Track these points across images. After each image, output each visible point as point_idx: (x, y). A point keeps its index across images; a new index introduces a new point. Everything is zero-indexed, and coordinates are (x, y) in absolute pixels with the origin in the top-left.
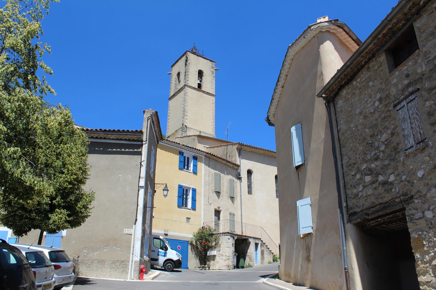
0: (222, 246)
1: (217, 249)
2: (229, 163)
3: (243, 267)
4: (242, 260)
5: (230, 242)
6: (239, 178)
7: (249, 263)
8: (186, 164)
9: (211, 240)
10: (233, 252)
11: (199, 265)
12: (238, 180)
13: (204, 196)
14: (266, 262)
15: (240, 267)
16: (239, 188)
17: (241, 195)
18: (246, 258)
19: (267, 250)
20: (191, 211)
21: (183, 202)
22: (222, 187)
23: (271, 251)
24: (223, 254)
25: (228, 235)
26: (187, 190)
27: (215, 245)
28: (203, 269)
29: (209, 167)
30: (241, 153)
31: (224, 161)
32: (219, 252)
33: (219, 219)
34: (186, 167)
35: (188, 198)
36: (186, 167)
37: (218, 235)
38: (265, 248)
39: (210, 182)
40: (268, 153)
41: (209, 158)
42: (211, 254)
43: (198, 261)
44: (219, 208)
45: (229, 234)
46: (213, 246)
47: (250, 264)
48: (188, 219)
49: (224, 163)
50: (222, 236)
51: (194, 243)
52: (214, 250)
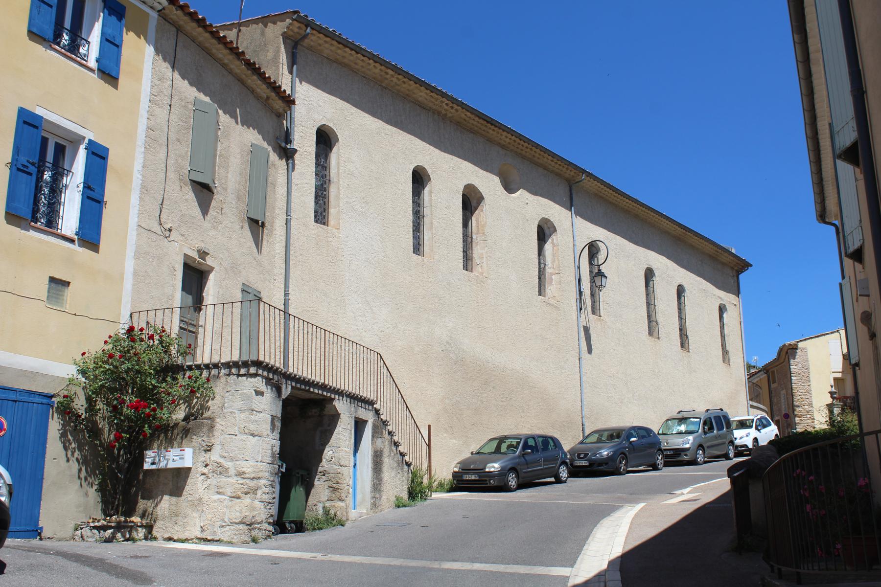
0: (220, 424)
1: (196, 440)
2: (255, 77)
3: (299, 528)
4: (297, 492)
5: (262, 407)
6: (288, 154)
7: (328, 504)
8: (67, 23)
9: (169, 394)
10: (273, 456)
11: (99, 515)
12: (281, 158)
13: (145, 189)
14: (388, 500)
15: (291, 522)
16: (281, 191)
17: (287, 222)
18: (316, 483)
19: (391, 450)
20: (75, 247)
21: (36, 201)
22: (222, 171)
23: (402, 455)
24: (226, 464)
25: (256, 375)
26: (60, 150)
27: (186, 419)
28: (119, 535)
29: (173, 67)
30: (300, 59)
31: (238, 63)
32: (203, 457)
33: (198, 304)
34: (66, 37)
35: (66, 186)
36: (66, 37)
37: (205, 373)
38: (386, 444)
39: (172, 136)
40: (395, 80)
41: (179, 29)
42: (162, 465)
43: (93, 495)
44: (203, 254)
45: (260, 372)
46: (176, 425)
47: (332, 512)
48: (58, 284)
49: (238, 71)
50: (223, 380)
51: (80, 404)
52: (180, 445)
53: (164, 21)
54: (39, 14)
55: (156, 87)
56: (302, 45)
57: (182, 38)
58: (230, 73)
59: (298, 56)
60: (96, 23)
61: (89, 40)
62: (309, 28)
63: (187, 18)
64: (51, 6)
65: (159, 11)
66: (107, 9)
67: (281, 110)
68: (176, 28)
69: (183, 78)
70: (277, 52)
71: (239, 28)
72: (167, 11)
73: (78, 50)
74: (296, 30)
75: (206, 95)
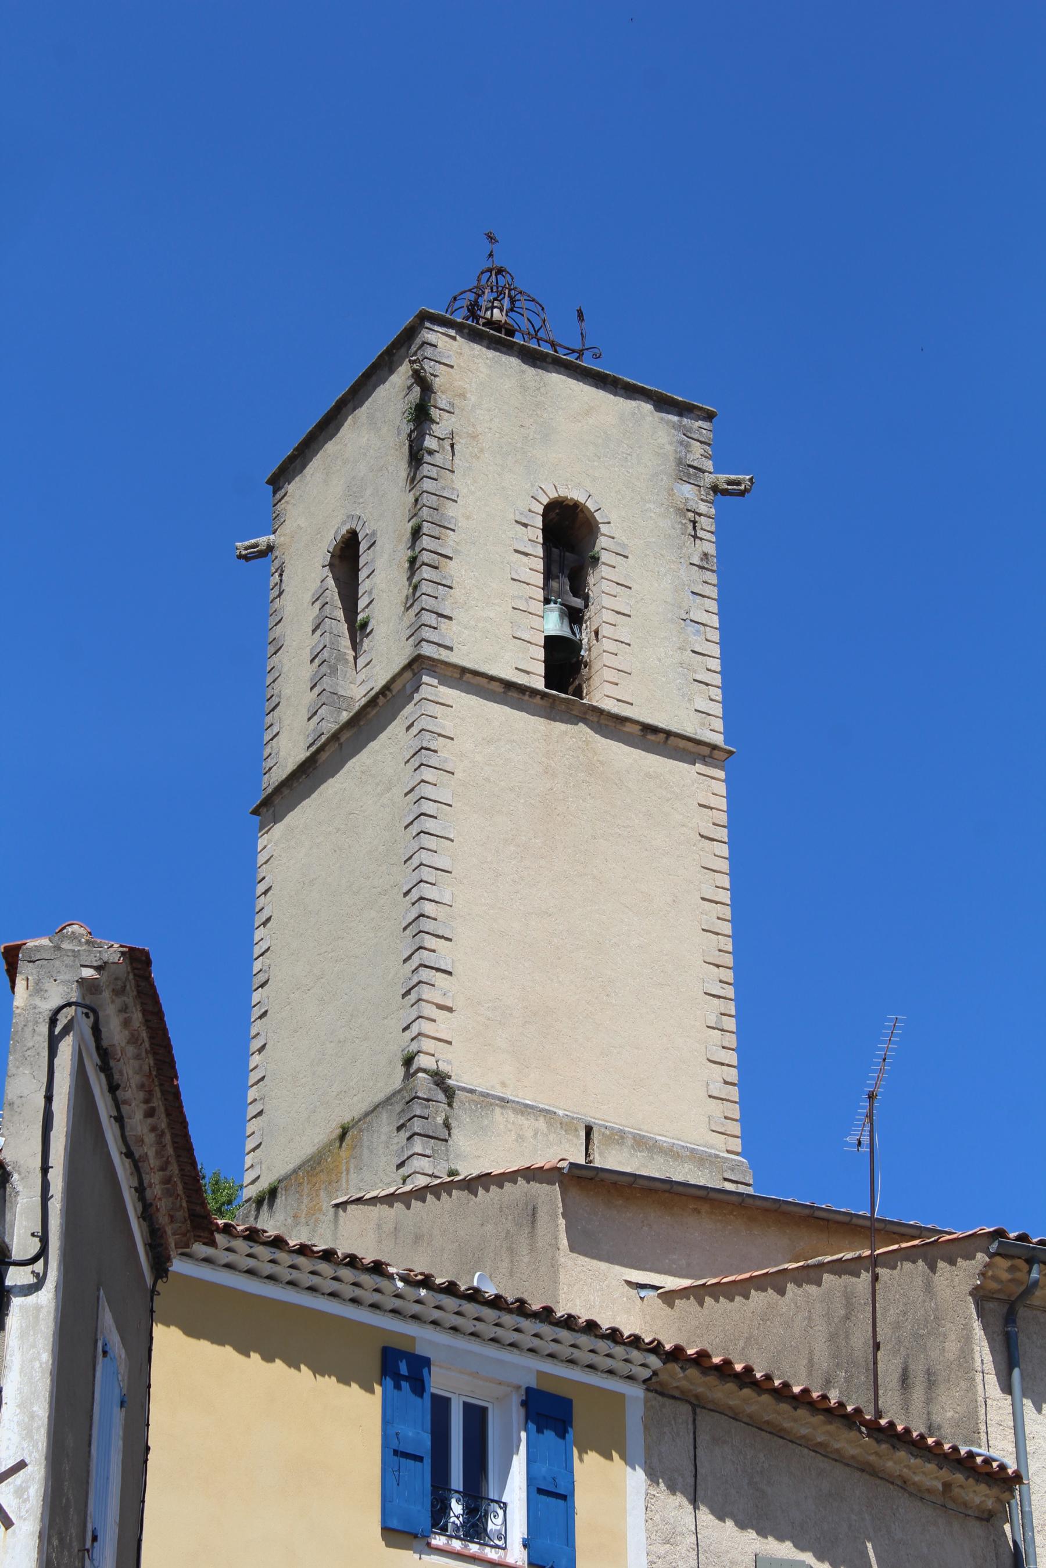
2: (902, 1454)
29: (694, 1502)
30: (1027, 1346)
36: (457, 1508)
41: (696, 1404)
49: (852, 1451)
53: (660, 1398)
54: (398, 1485)
55: (660, 1561)
56: (1030, 1307)
57: (705, 1420)
58: (836, 1460)
59: (1022, 1338)
60: (515, 1456)
61: (503, 1500)
62: (1035, 1267)
63: (712, 1379)
64: (419, 1459)
65: (645, 1381)
66: (533, 1422)
67: (990, 1504)
68: (691, 1403)
69: (721, 1518)
70: (967, 1340)
71: (874, 1271)
72: (663, 1377)
73: (485, 1530)
74: (1005, 1276)
75: (781, 1538)
